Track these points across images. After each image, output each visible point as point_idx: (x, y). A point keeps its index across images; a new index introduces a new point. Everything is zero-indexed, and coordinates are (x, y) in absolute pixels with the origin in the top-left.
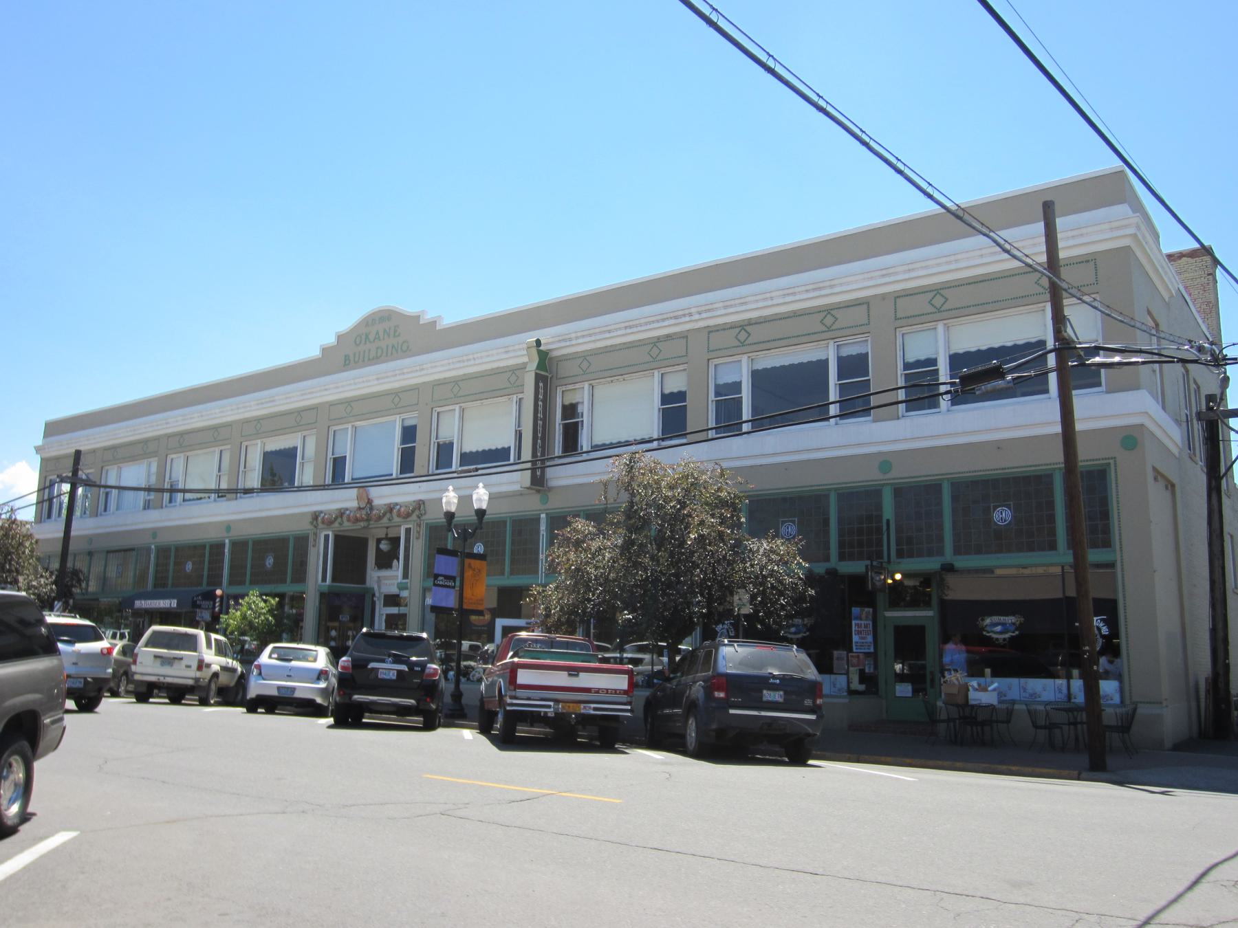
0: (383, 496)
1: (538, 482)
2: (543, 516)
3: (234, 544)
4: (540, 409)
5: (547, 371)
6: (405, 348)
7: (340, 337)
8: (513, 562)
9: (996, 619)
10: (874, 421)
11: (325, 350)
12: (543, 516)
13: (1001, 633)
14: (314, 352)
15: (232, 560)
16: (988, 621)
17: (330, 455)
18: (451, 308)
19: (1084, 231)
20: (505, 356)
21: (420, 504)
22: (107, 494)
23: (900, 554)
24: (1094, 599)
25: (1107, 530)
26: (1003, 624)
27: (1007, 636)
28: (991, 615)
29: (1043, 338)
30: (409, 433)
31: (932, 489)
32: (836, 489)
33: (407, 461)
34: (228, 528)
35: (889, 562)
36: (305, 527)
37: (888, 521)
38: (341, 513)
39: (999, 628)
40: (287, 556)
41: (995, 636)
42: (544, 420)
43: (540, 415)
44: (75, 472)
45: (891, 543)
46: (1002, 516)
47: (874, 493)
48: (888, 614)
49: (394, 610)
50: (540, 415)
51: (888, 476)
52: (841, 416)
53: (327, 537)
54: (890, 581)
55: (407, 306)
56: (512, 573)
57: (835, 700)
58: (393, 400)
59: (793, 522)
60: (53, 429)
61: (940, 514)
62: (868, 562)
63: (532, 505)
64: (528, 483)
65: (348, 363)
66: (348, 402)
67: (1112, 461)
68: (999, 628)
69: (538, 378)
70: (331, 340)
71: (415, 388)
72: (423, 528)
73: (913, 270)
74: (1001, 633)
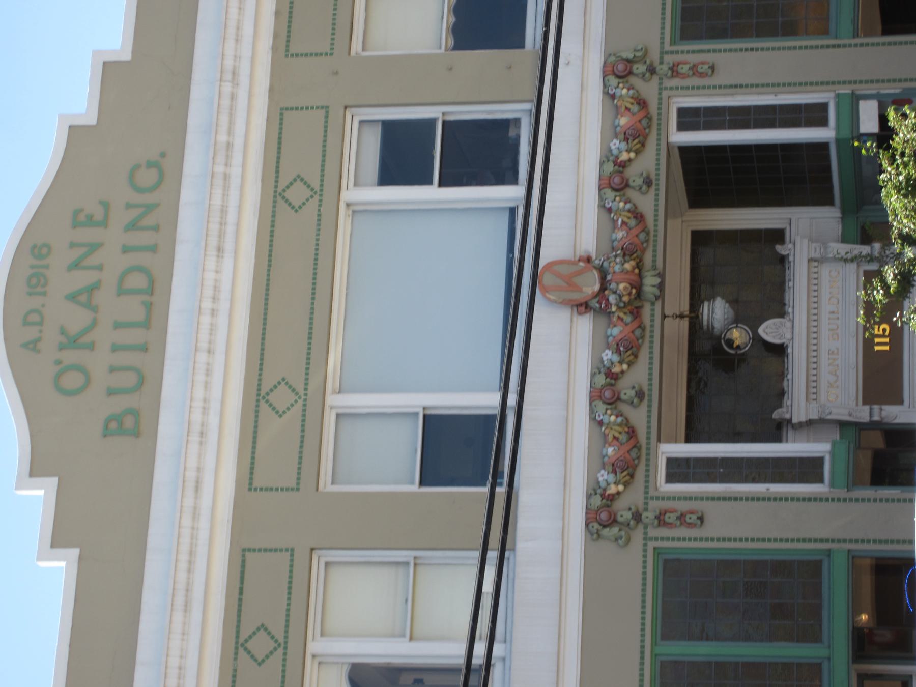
0: (574, 221)
6: (147, 177)
14: (59, 571)
19: (174, 662)
20: (228, 262)
21: (619, 69)
24: (830, 202)
29: (345, 669)
30: (403, 156)
33: (481, 153)
36: (633, 568)
38: (607, 391)
40: (720, 667)
53: (680, 470)
58: (295, 199)
65: (132, 424)
66: (258, 398)
71: (280, 116)
72: (695, 52)
73: (216, 288)
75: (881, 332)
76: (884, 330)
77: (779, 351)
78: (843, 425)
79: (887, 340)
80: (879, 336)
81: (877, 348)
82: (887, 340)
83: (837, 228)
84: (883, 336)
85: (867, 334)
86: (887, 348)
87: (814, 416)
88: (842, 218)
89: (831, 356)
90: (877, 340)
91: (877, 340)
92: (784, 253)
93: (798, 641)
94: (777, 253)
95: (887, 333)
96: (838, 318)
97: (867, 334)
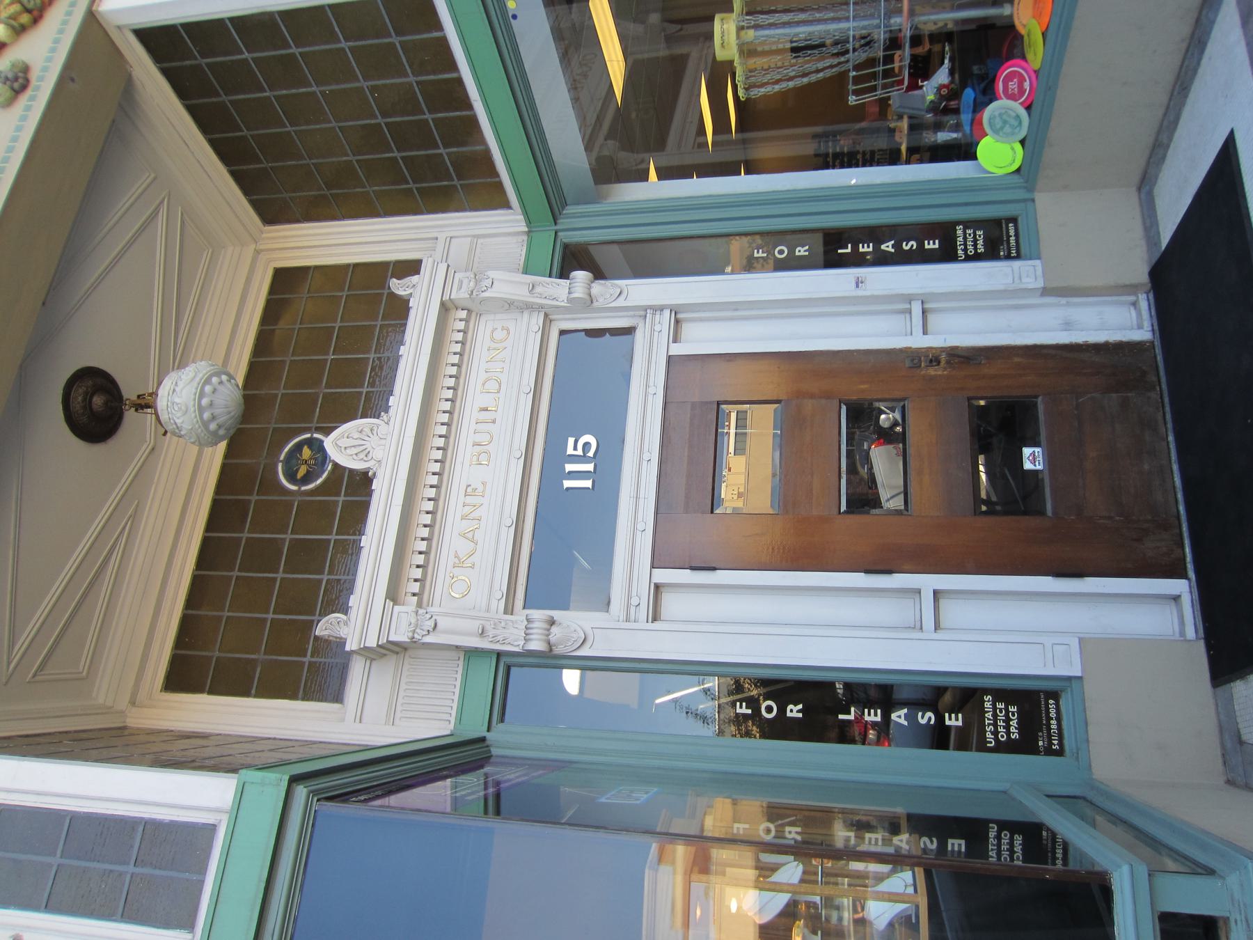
75: (580, 452)
76: (587, 446)
77: (362, 482)
78: (471, 654)
79: (589, 467)
80: (574, 459)
81: (567, 484)
82: (589, 467)
83: (516, 249)
84: (583, 459)
85: (998, 508)
86: (588, 484)
87: (401, 636)
88: (529, 233)
89: (469, 500)
90: (569, 467)
91: (569, 467)
92: (401, 292)
93: (864, 165)
94: (392, 296)
95: (591, 454)
96: (494, 422)
97: (998, 508)
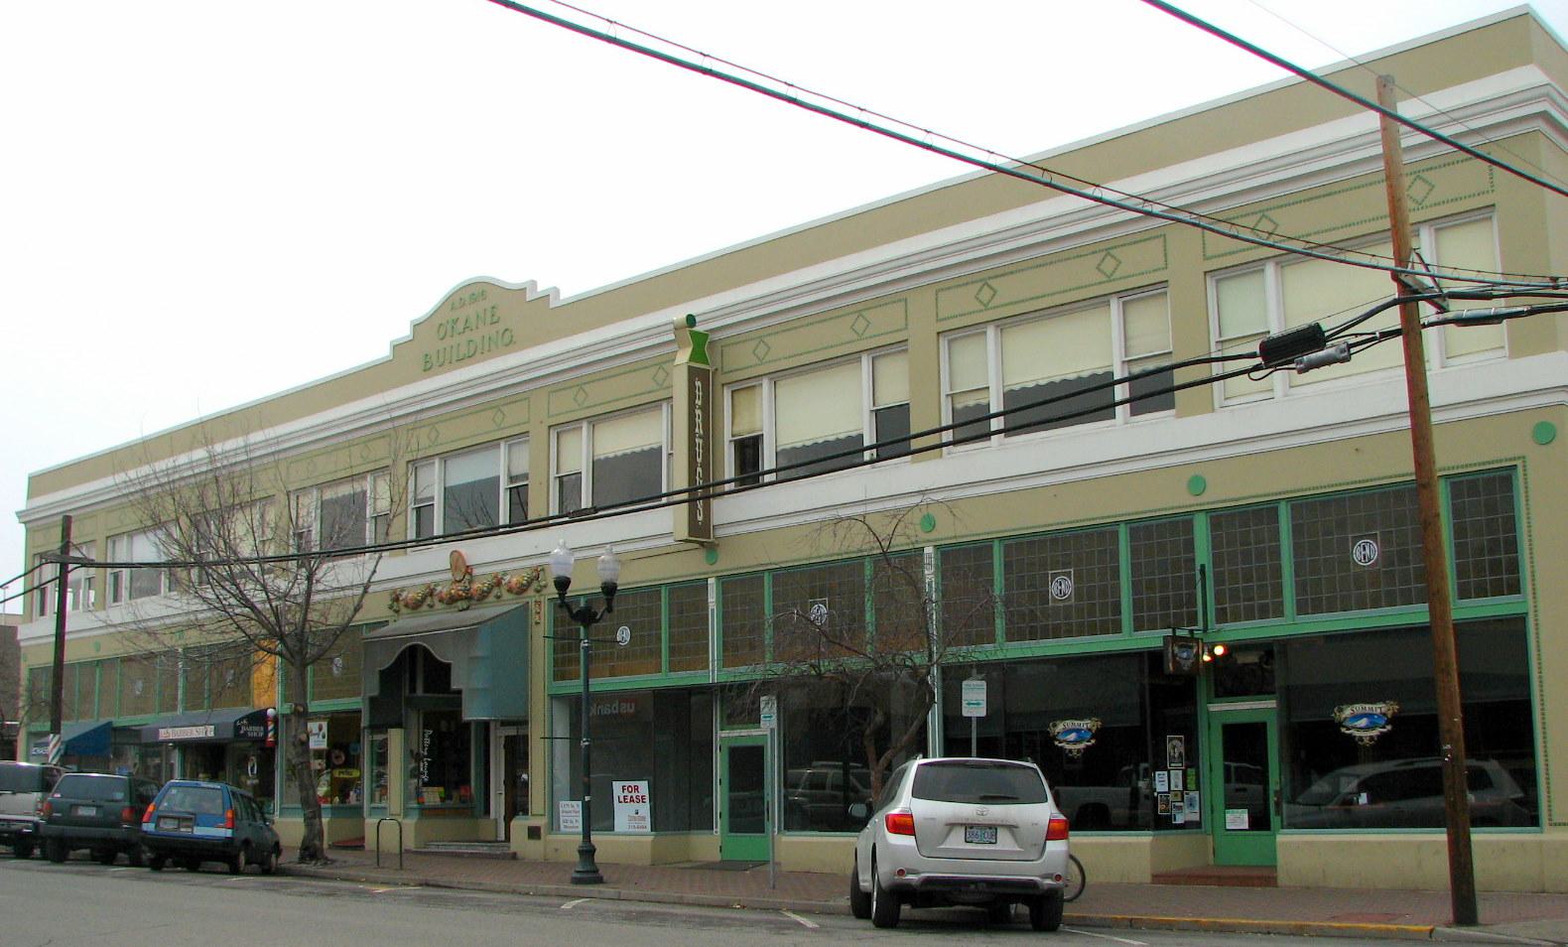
1: (701, 532)
2: (929, 550)
3: (950, 554)
4: (699, 421)
5: (67, 521)
6: (507, 339)
7: (417, 326)
8: (672, 651)
9: (1358, 708)
10: (1178, 416)
11: (397, 347)
12: (929, 550)
13: (1075, 742)
14: (383, 352)
15: (726, 616)
16: (1348, 712)
17: (553, 474)
18: (572, 277)
22: (116, 577)
23: (1222, 617)
25: (1514, 567)
26: (1078, 731)
27: (1375, 733)
28: (1063, 719)
31: (1262, 513)
32: (1127, 522)
34: (1197, 485)
35: (1205, 630)
37: (1203, 566)
39: (1363, 722)
41: (1357, 734)
42: (705, 437)
43: (699, 431)
44: (66, 546)
45: (1207, 598)
46: (1366, 553)
47: (1178, 525)
48: (1214, 707)
49: (512, 731)
50: (699, 431)
51: (1200, 500)
52: (1007, 431)
54: (1206, 658)
55: (511, 275)
56: (673, 668)
57: (628, 838)
59: (1068, 574)
60: (38, 483)
61: (1276, 553)
62: (1169, 632)
63: (690, 566)
64: (683, 532)
67: (1518, 462)
68: (1363, 722)
69: (693, 374)
70: (404, 332)
74: (1075, 742)
